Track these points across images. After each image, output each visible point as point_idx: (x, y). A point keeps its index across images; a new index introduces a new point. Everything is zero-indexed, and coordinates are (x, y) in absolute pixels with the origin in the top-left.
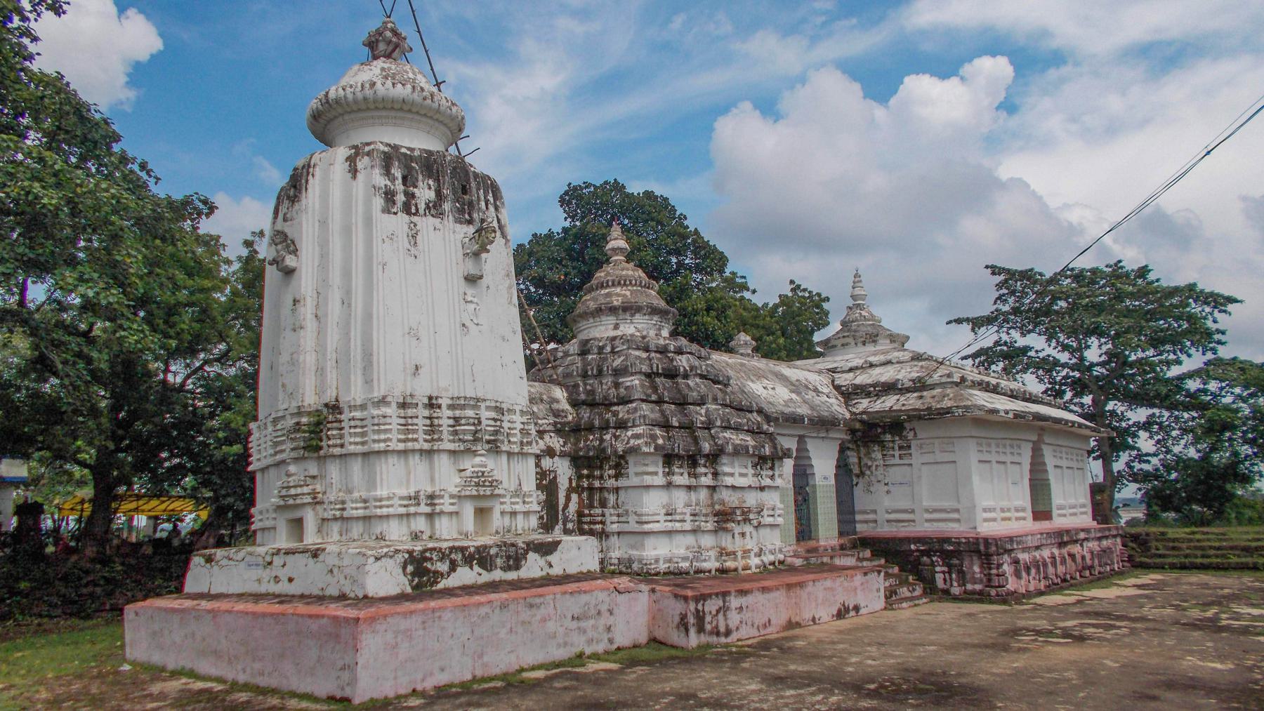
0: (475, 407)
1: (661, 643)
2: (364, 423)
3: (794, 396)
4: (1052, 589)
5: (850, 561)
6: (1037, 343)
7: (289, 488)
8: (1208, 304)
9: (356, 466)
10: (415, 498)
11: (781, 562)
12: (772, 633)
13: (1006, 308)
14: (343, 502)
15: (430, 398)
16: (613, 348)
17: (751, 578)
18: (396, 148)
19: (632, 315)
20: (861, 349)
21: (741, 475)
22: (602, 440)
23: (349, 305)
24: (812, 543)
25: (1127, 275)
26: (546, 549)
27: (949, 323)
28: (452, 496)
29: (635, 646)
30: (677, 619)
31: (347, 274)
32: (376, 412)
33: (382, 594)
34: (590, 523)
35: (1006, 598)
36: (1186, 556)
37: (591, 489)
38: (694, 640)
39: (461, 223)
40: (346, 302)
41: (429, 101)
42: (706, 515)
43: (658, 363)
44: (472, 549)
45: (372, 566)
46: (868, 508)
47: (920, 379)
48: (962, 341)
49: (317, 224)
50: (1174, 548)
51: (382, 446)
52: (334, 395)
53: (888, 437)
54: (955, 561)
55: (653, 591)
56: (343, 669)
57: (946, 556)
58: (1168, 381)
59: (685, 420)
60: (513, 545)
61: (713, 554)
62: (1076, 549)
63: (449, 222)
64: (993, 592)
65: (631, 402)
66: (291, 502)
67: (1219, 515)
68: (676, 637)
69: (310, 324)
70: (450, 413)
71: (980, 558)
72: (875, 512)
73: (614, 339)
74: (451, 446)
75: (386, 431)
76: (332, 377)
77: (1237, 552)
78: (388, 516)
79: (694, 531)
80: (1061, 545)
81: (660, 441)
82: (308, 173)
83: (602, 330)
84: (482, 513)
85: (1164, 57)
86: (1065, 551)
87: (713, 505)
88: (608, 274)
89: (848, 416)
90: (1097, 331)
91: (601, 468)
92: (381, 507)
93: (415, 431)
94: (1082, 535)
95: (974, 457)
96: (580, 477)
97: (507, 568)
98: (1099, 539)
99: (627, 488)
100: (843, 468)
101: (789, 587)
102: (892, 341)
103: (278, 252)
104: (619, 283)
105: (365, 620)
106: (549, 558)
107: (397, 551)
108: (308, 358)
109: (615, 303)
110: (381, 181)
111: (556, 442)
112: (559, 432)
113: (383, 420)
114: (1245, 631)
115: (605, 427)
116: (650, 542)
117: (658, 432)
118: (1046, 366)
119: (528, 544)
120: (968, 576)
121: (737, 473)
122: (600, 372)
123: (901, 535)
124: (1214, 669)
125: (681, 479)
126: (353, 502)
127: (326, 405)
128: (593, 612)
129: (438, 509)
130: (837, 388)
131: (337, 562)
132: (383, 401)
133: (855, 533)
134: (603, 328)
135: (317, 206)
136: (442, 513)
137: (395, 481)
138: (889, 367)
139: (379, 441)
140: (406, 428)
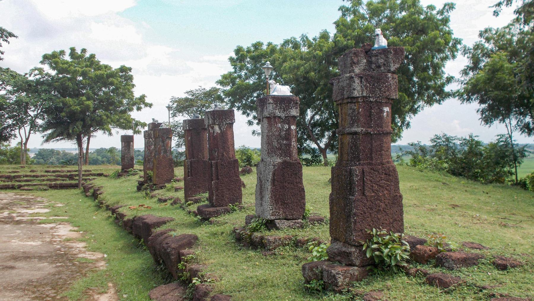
77: (3, 179)
114: (32, 222)
124: (31, 245)
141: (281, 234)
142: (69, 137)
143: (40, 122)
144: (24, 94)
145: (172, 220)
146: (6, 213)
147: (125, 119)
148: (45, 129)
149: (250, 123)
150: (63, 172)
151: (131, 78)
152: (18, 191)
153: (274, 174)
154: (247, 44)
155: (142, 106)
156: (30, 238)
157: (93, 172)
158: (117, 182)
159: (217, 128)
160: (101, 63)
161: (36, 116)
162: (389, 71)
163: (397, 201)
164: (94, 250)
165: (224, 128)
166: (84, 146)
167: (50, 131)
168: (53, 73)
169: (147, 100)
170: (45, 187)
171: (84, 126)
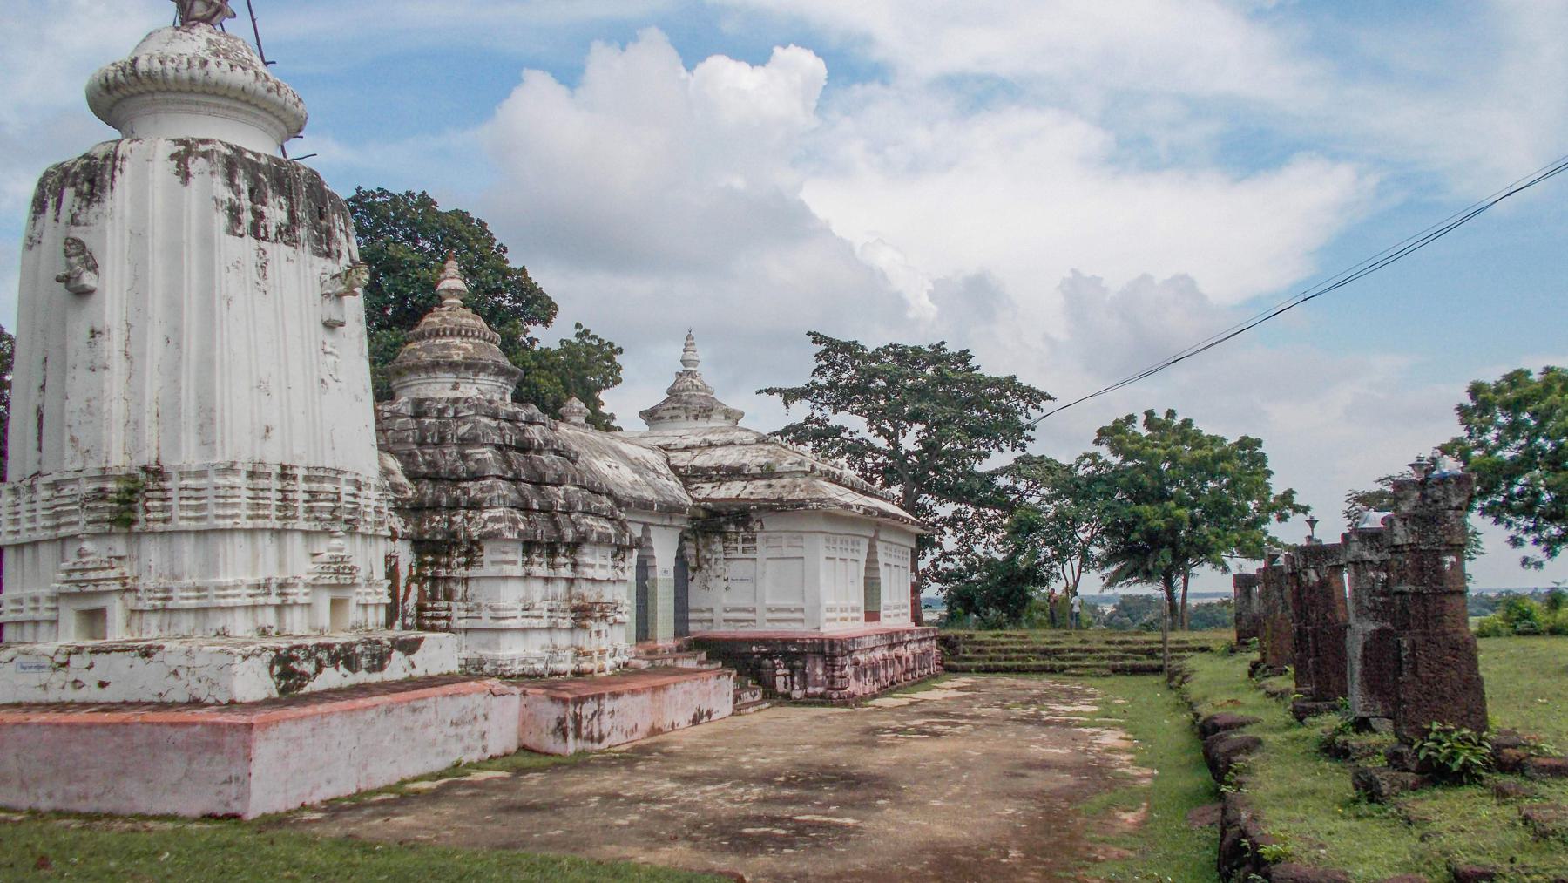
0: (335, 480)
1: (533, 751)
2: (201, 494)
3: (637, 477)
4: (885, 691)
5: (691, 664)
6: (855, 424)
7: (86, 570)
8: (1023, 398)
9: (187, 547)
10: (264, 587)
11: (625, 665)
12: (640, 739)
13: (823, 381)
14: (167, 590)
15: (284, 467)
16: (456, 412)
17: (607, 681)
18: (238, 151)
19: (476, 375)
20: (692, 423)
21: (602, 566)
22: (451, 523)
23: (179, 345)
24: (650, 644)
25: (948, 358)
26: (410, 647)
27: (760, 392)
28: (306, 585)
29: (506, 755)
30: (553, 724)
31: (174, 305)
32: (221, 481)
33: (250, 698)
34: (432, 618)
35: (848, 701)
36: (991, 660)
37: (435, 579)
38: (572, 746)
39: (319, 255)
40: (173, 340)
41: (274, 95)
42: (564, 611)
43: (510, 436)
44: (338, 647)
45: (240, 667)
46: (704, 605)
47: (769, 466)
48: (771, 416)
49: (127, 235)
50: (979, 651)
51: (229, 523)
52: (154, 456)
53: (732, 528)
54: (799, 664)
55: (524, 694)
56: (229, 781)
57: (789, 658)
58: (980, 476)
59: (544, 503)
60: (378, 642)
61: (569, 654)
62: (901, 651)
63: (305, 253)
64: (835, 695)
65: (484, 478)
66: (91, 588)
67: (1015, 618)
68: (551, 744)
69: (118, 365)
70: (304, 486)
71: (824, 659)
72: (711, 610)
73: (456, 401)
74: (305, 526)
75: (234, 505)
76: (150, 433)
78: (232, 608)
79: (549, 629)
80: (891, 646)
81: (522, 526)
82: (114, 168)
83: (439, 389)
84: (336, 604)
85: (978, 93)
86: (893, 653)
87: (570, 600)
88: (444, 320)
89: (690, 502)
90: (915, 417)
91: (448, 554)
92: (224, 597)
93: (267, 506)
94: (907, 637)
95: (823, 553)
96: (422, 564)
97: (371, 669)
98: (919, 641)
99: (478, 579)
100: (681, 558)
101: (655, 689)
102: (727, 418)
103: (70, 266)
104: (459, 333)
105: (259, 725)
106: (412, 657)
107: (264, 649)
108: (114, 406)
109: (456, 358)
110: (225, 194)
111: (397, 522)
112: (398, 510)
113: (230, 492)
114: (1066, 724)
115: (454, 506)
116: (506, 640)
117: (519, 516)
118: (857, 450)
119: (393, 641)
120: (810, 679)
121: (596, 563)
122: (442, 440)
123: (741, 636)
125: (540, 570)
126: (182, 589)
127: (145, 469)
128: (471, 717)
129: (290, 599)
130: (674, 469)
131: (183, 661)
132: (231, 469)
133: (688, 633)
134: (438, 386)
135: (128, 212)
136: (295, 604)
137: (240, 566)
138: (732, 449)
139: (224, 517)
140: (256, 502)
141: (1373, 739)
142: (1148, 576)
143: (1095, 551)
144: (1069, 501)
145: (1256, 721)
146: (1032, 710)
147: (1254, 540)
148: (1104, 565)
149: (1515, 542)
150: (1137, 643)
151: (1262, 459)
152: (1061, 676)
153: (1365, 648)
154: (1492, 375)
155: (1290, 512)
156: (1056, 744)
157: (1192, 644)
158: (1222, 664)
159: (1312, 575)
160: (1205, 434)
161: (1090, 541)
162: (1450, 508)
163: (1474, 685)
164: (1143, 765)
165: (1324, 573)
166: (1179, 591)
167: (1113, 568)
168: (1116, 460)
169: (1297, 500)
170: (1105, 672)
171: (1175, 556)
